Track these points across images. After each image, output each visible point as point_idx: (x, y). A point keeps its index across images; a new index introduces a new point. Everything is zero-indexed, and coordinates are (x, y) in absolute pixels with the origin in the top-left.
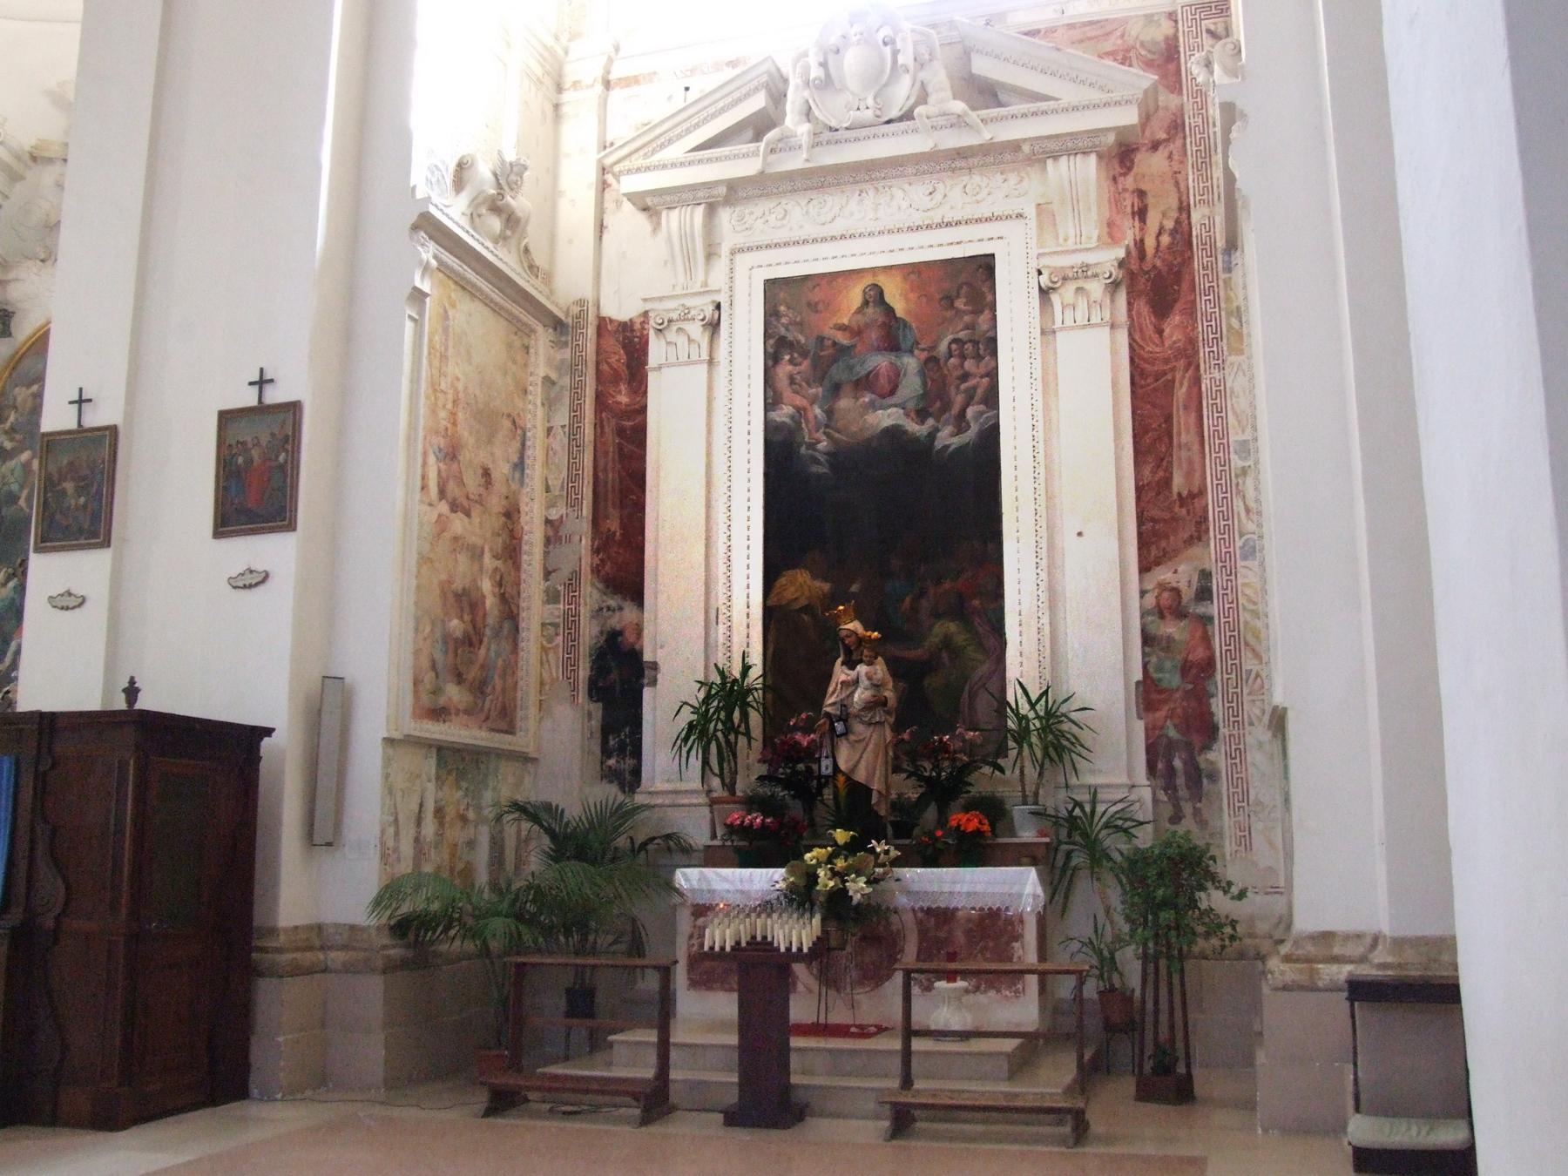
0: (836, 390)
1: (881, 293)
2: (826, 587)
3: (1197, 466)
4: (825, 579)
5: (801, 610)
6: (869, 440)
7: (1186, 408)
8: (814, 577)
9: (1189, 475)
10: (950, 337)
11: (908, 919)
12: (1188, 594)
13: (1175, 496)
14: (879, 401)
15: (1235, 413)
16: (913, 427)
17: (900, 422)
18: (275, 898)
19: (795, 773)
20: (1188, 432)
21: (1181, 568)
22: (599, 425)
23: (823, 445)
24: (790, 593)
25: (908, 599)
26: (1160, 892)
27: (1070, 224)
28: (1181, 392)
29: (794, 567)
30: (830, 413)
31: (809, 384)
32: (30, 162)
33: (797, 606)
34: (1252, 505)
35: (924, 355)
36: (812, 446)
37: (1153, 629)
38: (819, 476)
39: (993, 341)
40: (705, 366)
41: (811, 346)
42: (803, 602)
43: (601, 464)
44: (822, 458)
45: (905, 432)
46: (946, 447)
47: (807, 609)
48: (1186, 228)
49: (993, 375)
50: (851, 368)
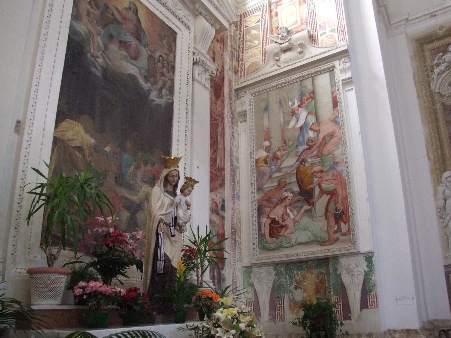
2: (93, 141)
3: (223, 159)
4: (92, 136)
7: (221, 136)
8: (86, 131)
10: (160, 54)
14: (129, 59)
17: (137, 76)
18: (427, 146)
21: (218, 195)
24: (69, 135)
25: (132, 167)
26: (282, 269)
27: (200, 44)
28: (220, 129)
29: (74, 119)
32: (302, 55)
33: (73, 144)
38: (95, 75)
39: (173, 67)
42: (77, 144)
44: (99, 68)
47: (80, 149)
49: (172, 81)
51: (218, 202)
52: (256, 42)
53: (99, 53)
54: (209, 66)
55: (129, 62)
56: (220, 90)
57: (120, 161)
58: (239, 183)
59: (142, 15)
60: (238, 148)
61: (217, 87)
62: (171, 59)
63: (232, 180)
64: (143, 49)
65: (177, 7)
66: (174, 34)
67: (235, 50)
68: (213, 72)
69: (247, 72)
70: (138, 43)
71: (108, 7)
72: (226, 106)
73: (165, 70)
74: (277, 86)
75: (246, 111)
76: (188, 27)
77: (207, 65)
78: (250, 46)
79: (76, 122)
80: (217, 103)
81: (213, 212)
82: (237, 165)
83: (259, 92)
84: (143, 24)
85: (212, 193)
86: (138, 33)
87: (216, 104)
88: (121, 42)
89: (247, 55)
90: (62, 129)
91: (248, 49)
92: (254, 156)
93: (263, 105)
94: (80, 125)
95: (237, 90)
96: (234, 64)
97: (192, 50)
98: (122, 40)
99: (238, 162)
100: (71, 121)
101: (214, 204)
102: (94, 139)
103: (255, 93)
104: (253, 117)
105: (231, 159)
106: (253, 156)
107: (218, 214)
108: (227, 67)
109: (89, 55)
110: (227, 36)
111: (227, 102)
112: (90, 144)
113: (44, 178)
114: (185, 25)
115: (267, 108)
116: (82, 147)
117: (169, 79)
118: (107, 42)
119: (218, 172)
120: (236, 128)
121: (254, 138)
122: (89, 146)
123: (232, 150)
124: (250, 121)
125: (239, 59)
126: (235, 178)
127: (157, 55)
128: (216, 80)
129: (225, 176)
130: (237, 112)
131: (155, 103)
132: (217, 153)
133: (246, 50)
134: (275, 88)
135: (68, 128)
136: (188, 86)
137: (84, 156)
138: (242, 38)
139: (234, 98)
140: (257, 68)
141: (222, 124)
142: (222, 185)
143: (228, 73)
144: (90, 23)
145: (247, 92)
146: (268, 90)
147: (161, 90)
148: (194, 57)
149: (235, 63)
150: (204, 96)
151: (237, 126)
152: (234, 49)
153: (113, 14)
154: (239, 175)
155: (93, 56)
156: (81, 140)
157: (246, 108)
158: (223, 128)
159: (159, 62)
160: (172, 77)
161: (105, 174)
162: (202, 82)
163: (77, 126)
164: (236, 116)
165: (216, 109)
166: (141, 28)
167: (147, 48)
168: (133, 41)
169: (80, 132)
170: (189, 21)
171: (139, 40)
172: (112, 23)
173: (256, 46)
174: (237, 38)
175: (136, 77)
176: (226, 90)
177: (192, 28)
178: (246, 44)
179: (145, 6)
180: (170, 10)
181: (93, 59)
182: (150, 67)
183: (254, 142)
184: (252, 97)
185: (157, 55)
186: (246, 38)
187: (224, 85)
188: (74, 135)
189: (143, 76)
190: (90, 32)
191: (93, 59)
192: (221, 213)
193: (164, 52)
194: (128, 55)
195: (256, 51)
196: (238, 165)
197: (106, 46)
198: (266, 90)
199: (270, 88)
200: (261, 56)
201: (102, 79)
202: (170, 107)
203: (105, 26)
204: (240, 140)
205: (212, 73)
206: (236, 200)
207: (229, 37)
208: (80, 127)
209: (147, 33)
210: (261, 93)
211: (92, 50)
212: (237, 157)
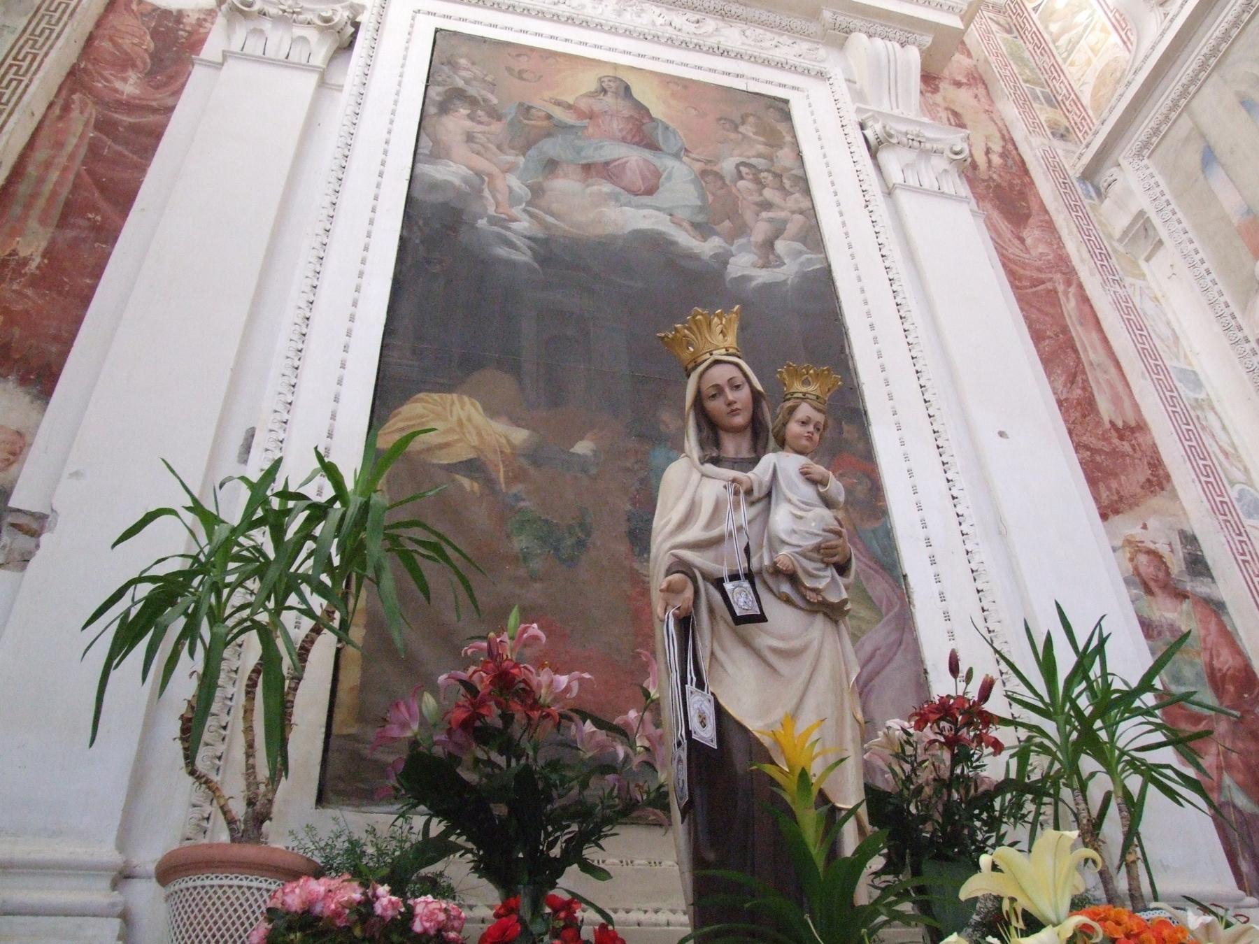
0: (551, 166)
1: (627, 89)
2: (520, 436)
4: (516, 422)
5: (451, 468)
6: (613, 238)
8: (492, 412)
9: (1116, 400)
10: (738, 160)
11: (498, 458)
12: (1176, 564)
13: (1108, 425)
14: (625, 197)
15: (1159, 337)
16: (686, 240)
17: (662, 228)
19: (365, 908)
20: (1095, 351)
21: (1153, 523)
22: (61, 105)
23: (523, 225)
28: (1070, 306)
30: (537, 191)
31: (499, 147)
33: (444, 458)
34: (1229, 449)
35: (698, 166)
36: (504, 222)
37: (1146, 613)
38: (511, 264)
40: (313, 79)
41: (510, 111)
42: (462, 453)
43: (40, 155)
44: (519, 242)
45: (674, 243)
46: (745, 279)
47: (473, 467)
48: (1017, 158)
49: (811, 213)
50: (579, 150)
51: (1163, 549)
52: (1081, 18)
53: (516, 211)
54: (932, 140)
55: (629, 204)
56: (1022, 195)
57: (642, 474)
58: (1239, 457)
59: (645, 93)
60: (1176, 338)
61: (1005, 194)
62: (784, 157)
63: (1195, 452)
64: (670, 163)
65: (767, 44)
66: (781, 105)
67: (1033, 83)
68: (957, 149)
69: (1098, 109)
70: (648, 154)
71: (529, 108)
72: (1064, 233)
73: (769, 194)
74: (1203, 66)
75: (1141, 213)
76: (821, 75)
77: (928, 140)
78: (1070, 41)
79: (455, 396)
80: (1025, 234)
81: (1149, 591)
82: (1192, 395)
83: (1156, 131)
84: (657, 110)
85: (1116, 520)
86: (643, 130)
87: (1022, 240)
88: (587, 168)
89: (1073, 70)
90: (401, 425)
91: (1069, 55)
92: (1246, 331)
93: (1192, 158)
94: (466, 398)
95: (1089, 175)
96: (1043, 119)
97: (852, 118)
98: (590, 161)
99: (1197, 384)
100: (436, 396)
101: (1143, 559)
102: (526, 427)
103: (1146, 145)
104: (1180, 215)
105: (1158, 383)
106: (1240, 335)
107: (1182, 596)
108: (1019, 134)
109: (482, 223)
110: (986, 61)
111: (1062, 220)
112: (513, 447)
113: (600, 905)
114: (806, 72)
115: (1209, 157)
116: (478, 459)
117: (793, 212)
118: (540, 179)
119: (1116, 441)
120: (1139, 283)
121: (1214, 275)
122: (508, 451)
123: (1148, 354)
124: (1170, 235)
125: (1060, 98)
126: (1207, 440)
127: (727, 166)
128: (995, 176)
129: (1161, 449)
130: (1117, 233)
131: (754, 283)
132: (1086, 381)
133: (1065, 60)
134: (1203, 75)
135: (422, 416)
136: (870, 208)
137: (489, 482)
138: (1041, 46)
139: (1086, 201)
140: (1118, 74)
141: (1072, 290)
142: (1158, 480)
143: (1029, 143)
144: (478, 154)
145: (1121, 161)
146: (1183, 102)
147: (769, 245)
148: (869, 133)
149: (1045, 114)
150: (958, 237)
151: (1142, 276)
152: (1026, 81)
153: (549, 117)
154: (1224, 428)
155: (493, 221)
156: (474, 440)
157: (1142, 201)
158: (1085, 300)
159: (741, 178)
160: (805, 204)
161: (581, 525)
162: (926, 185)
163: (457, 405)
164: (1120, 248)
165: (1027, 251)
166: (652, 119)
167: (685, 159)
168: (634, 157)
169: (469, 420)
170: (823, 61)
171: (653, 147)
172: (549, 135)
173: (1087, 26)
174: (1027, 55)
175: (660, 233)
176: (1045, 188)
177: (837, 73)
178: (1057, 48)
179: (651, 72)
180: (739, 56)
181: (496, 229)
182: (710, 198)
183: (1220, 286)
184: (1146, 161)
185: (727, 166)
186: (1051, 34)
187: (1032, 183)
188: (450, 431)
189: (685, 224)
190: (478, 174)
191: (496, 229)
192: (1200, 587)
193: (754, 153)
194: (618, 189)
195: (1092, 38)
196: (1202, 396)
197: (537, 191)
198: (1175, 105)
199: (1184, 93)
200: (1114, 38)
201: (536, 265)
202: (821, 287)
203: (524, 150)
204: (1170, 316)
205: (956, 153)
206: (1247, 522)
207: (992, 59)
208: (468, 406)
209: (672, 125)
210: (1164, 128)
211: (491, 210)
212: (1182, 371)
